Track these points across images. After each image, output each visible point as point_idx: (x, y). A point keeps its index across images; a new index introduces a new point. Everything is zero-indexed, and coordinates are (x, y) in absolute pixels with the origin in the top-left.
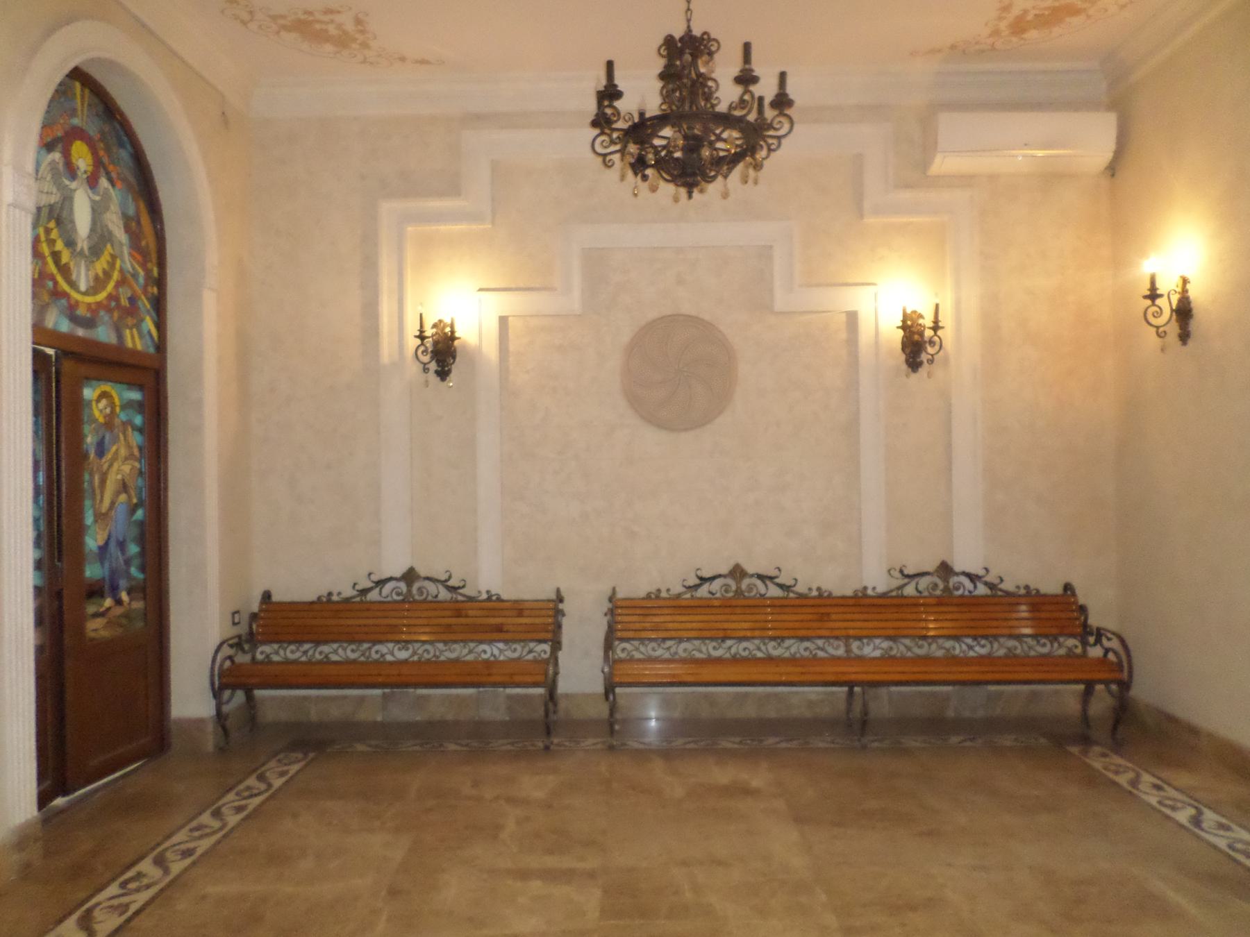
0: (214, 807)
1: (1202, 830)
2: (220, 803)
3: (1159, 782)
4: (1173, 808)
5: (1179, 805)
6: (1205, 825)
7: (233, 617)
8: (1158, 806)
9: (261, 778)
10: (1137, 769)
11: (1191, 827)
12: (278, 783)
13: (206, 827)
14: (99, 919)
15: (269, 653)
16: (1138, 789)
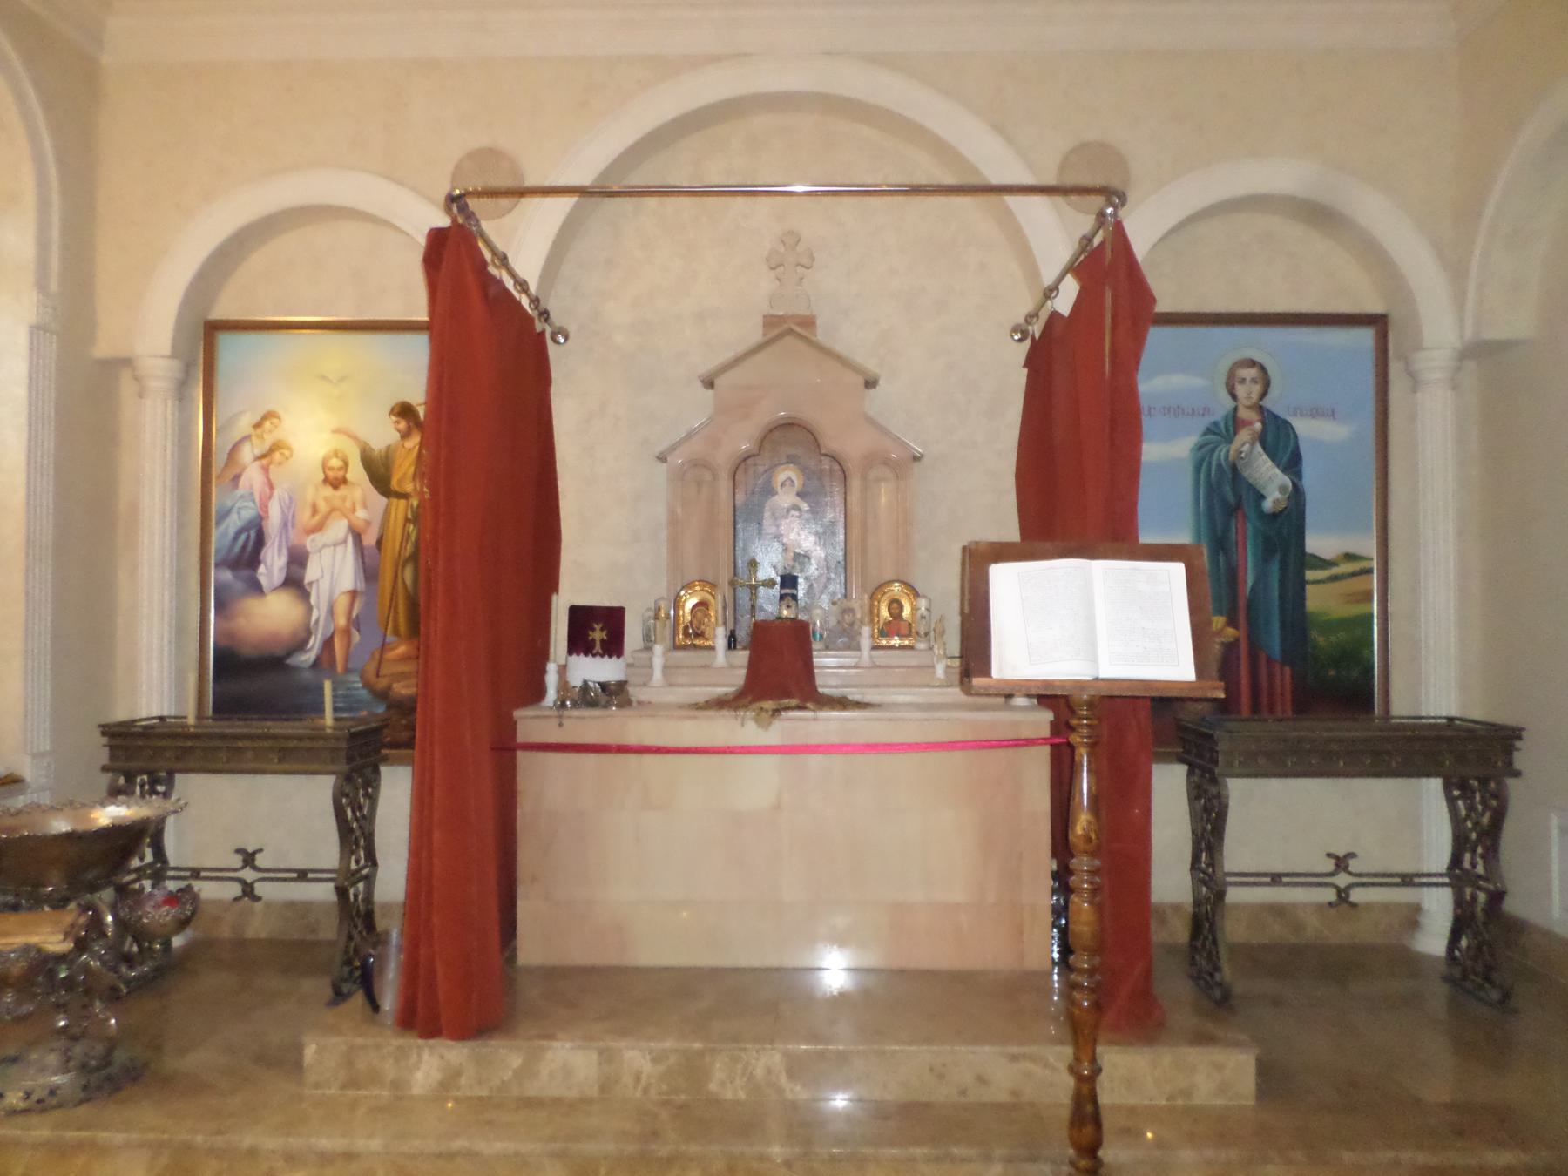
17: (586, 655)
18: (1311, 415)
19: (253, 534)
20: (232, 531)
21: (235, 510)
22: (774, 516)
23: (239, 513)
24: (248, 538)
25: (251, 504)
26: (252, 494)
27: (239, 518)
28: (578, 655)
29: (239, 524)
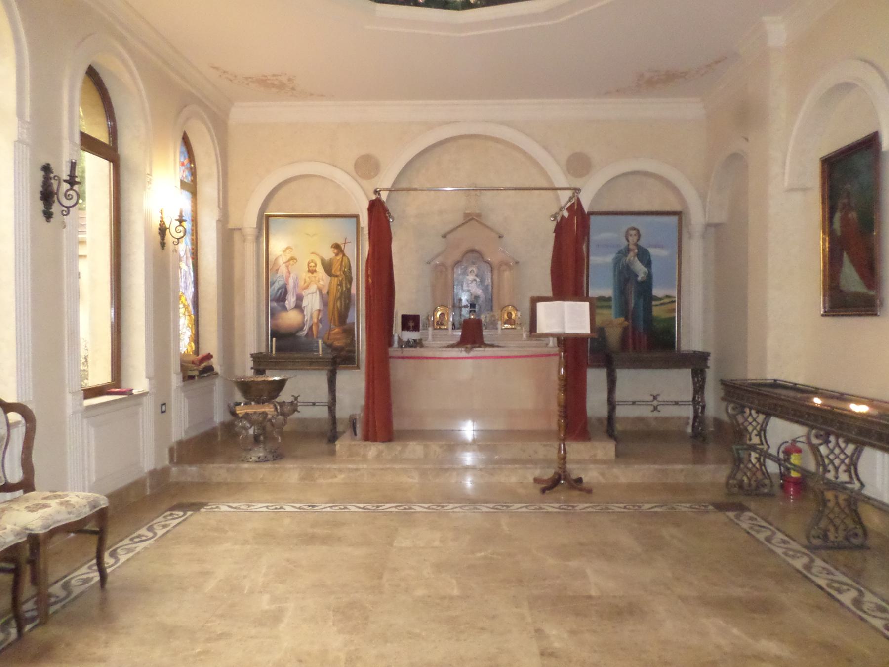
0: (111, 550)
1: (812, 573)
2: (117, 546)
3: (786, 538)
4: (839, 591)
5: (845, 587)
6: (865, 607)
7: (162, 408)
8: (783, 556)
9: (150, 529)
10: (812, 555)
11: (852, 607)
12: (160, 532)
13: (143, 536)
14: (121, 553)
15: (296, 396)
16: (740, 520)
19: (283, 290)
20: (276, 288)
21: (277, 281)
23: (278, 282)
25: (283, 279)
26: (283, 276)
29: (278, 286)
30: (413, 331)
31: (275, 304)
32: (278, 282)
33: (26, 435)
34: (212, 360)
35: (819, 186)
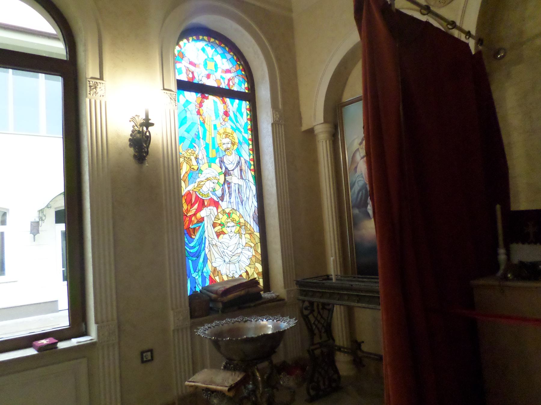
17: (523, 243)
18: (197, 257)
19: (364, 191)
20: (356, 191)
21: (357, 181)
22: (192, 224)
23: (358, 184)
24: (362, 194)
25: (362, 179)
26: (362, 174)
27: (358, 186)
28: (517, 243)
29: (359, 188)
30: (535, 243)
31: (356, 211)
32: (358, 184)
33: (213, 31)
34: (205, 100)
35: (361, 70)
